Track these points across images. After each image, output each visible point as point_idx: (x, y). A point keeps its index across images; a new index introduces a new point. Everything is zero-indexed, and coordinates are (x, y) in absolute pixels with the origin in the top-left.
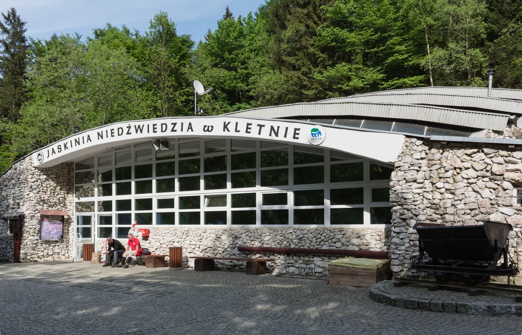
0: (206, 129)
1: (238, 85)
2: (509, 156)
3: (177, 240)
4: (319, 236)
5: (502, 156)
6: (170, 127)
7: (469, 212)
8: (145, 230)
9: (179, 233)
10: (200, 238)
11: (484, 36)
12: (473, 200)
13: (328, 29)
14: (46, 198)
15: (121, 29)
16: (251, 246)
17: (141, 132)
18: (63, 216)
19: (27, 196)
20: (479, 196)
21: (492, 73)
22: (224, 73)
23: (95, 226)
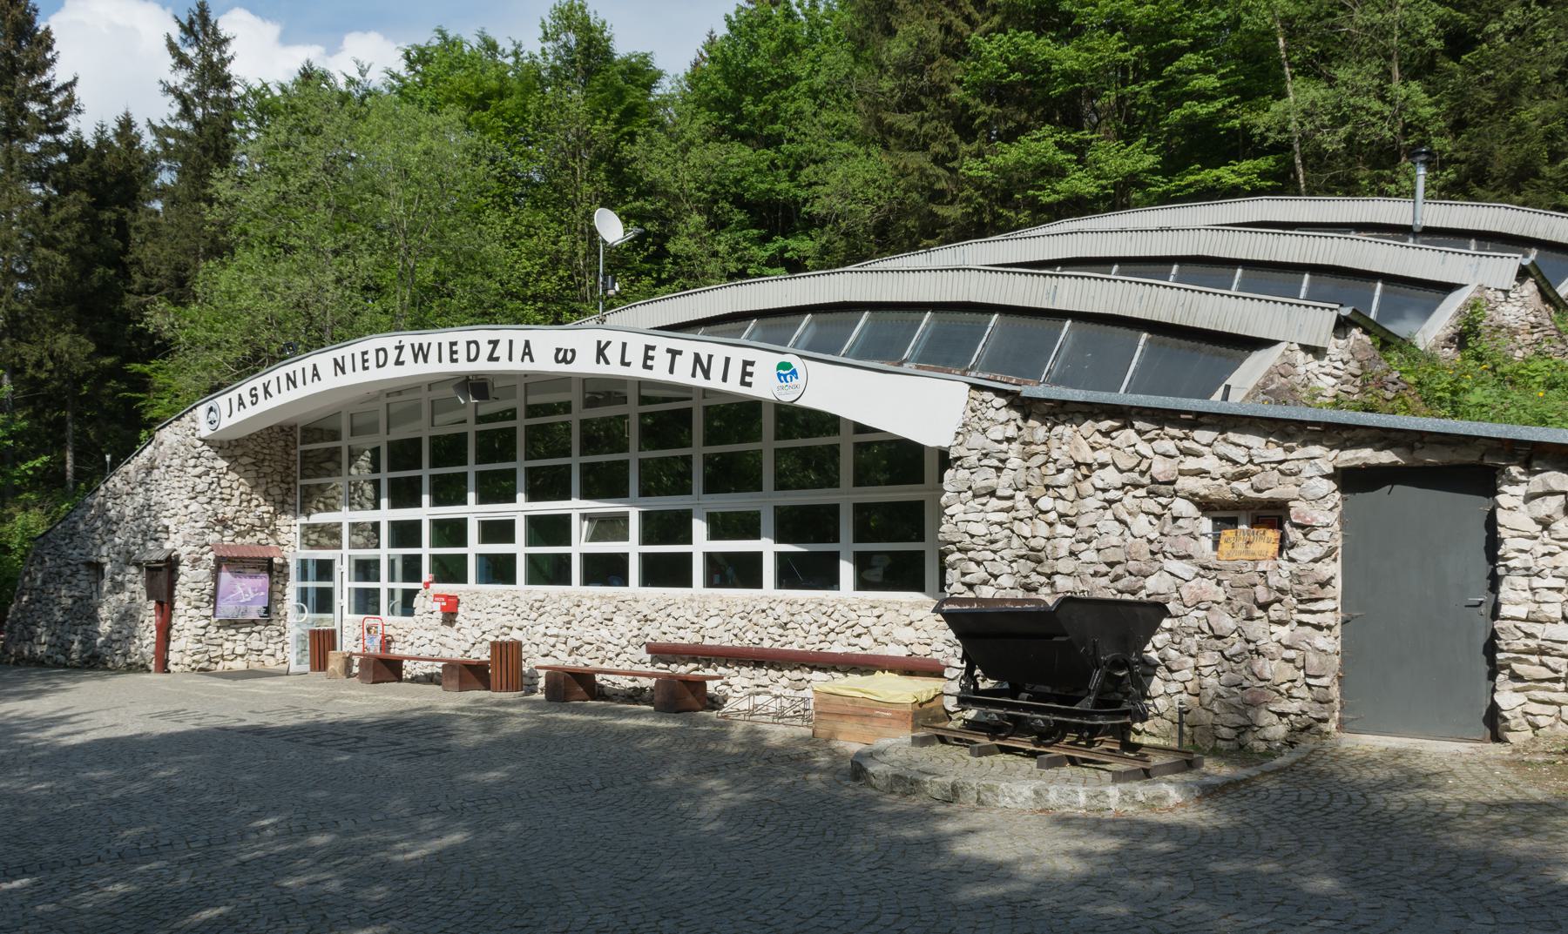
1: (778, 187)
2: (1187, 438)
3: (519, 623)
5: (1173, 438)
6: (486, 349)
7: (1104, 569)
8: (447, 597)
9: (522, 607)
10: (567, 619)
11: (1437, 44)
12: (1115, 540)
13: (1000, 35)
14: (229, 515)
15: (475, 42)
16: (679, 641)
18: (270, 560)
19: (184, 511)
20: (1127, 533)
21: (1423, 158)
22: (741, 153)
23: (344, 585)
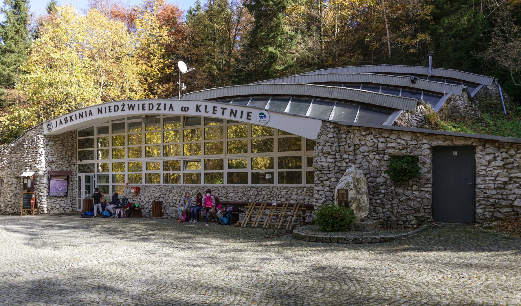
0: (183, 109)
4: (269, 193)
5: (384, 137)
17: (133, 109)
